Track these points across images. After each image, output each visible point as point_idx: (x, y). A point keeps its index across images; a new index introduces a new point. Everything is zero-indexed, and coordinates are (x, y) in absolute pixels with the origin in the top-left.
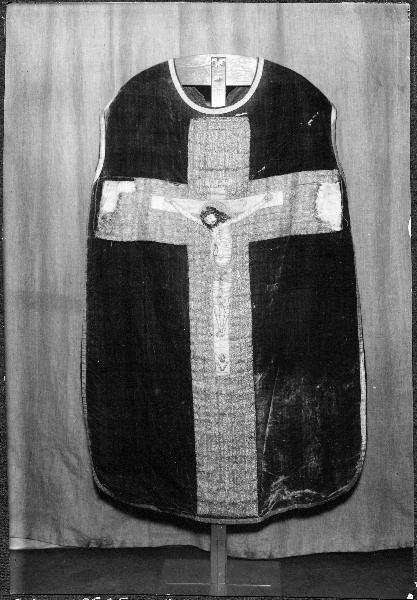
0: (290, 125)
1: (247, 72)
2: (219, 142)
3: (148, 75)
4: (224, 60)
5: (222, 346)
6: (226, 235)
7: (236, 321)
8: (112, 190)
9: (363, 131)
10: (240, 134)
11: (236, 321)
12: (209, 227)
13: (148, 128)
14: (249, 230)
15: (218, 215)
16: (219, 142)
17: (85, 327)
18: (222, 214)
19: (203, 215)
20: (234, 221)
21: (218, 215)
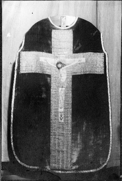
0: (87, 37)
1: (72, 21)
2: (63, 39)
3: (39, 23)
4: (65, 19)
5: (61, 103)
6: (65, 71)
7: (66, 102)
8: (24, 54)
9: (110, 36)
10: (69, 36)
11: (66, 102)
12: (59, 68)
13: (39, 37)
14: (71, 70)
15: (62, 63)
16: (63, 39)
17: (120, 114)
18: (63, 64)
19: (58, 63)
20: (67, 66)
21: (62, 63)
